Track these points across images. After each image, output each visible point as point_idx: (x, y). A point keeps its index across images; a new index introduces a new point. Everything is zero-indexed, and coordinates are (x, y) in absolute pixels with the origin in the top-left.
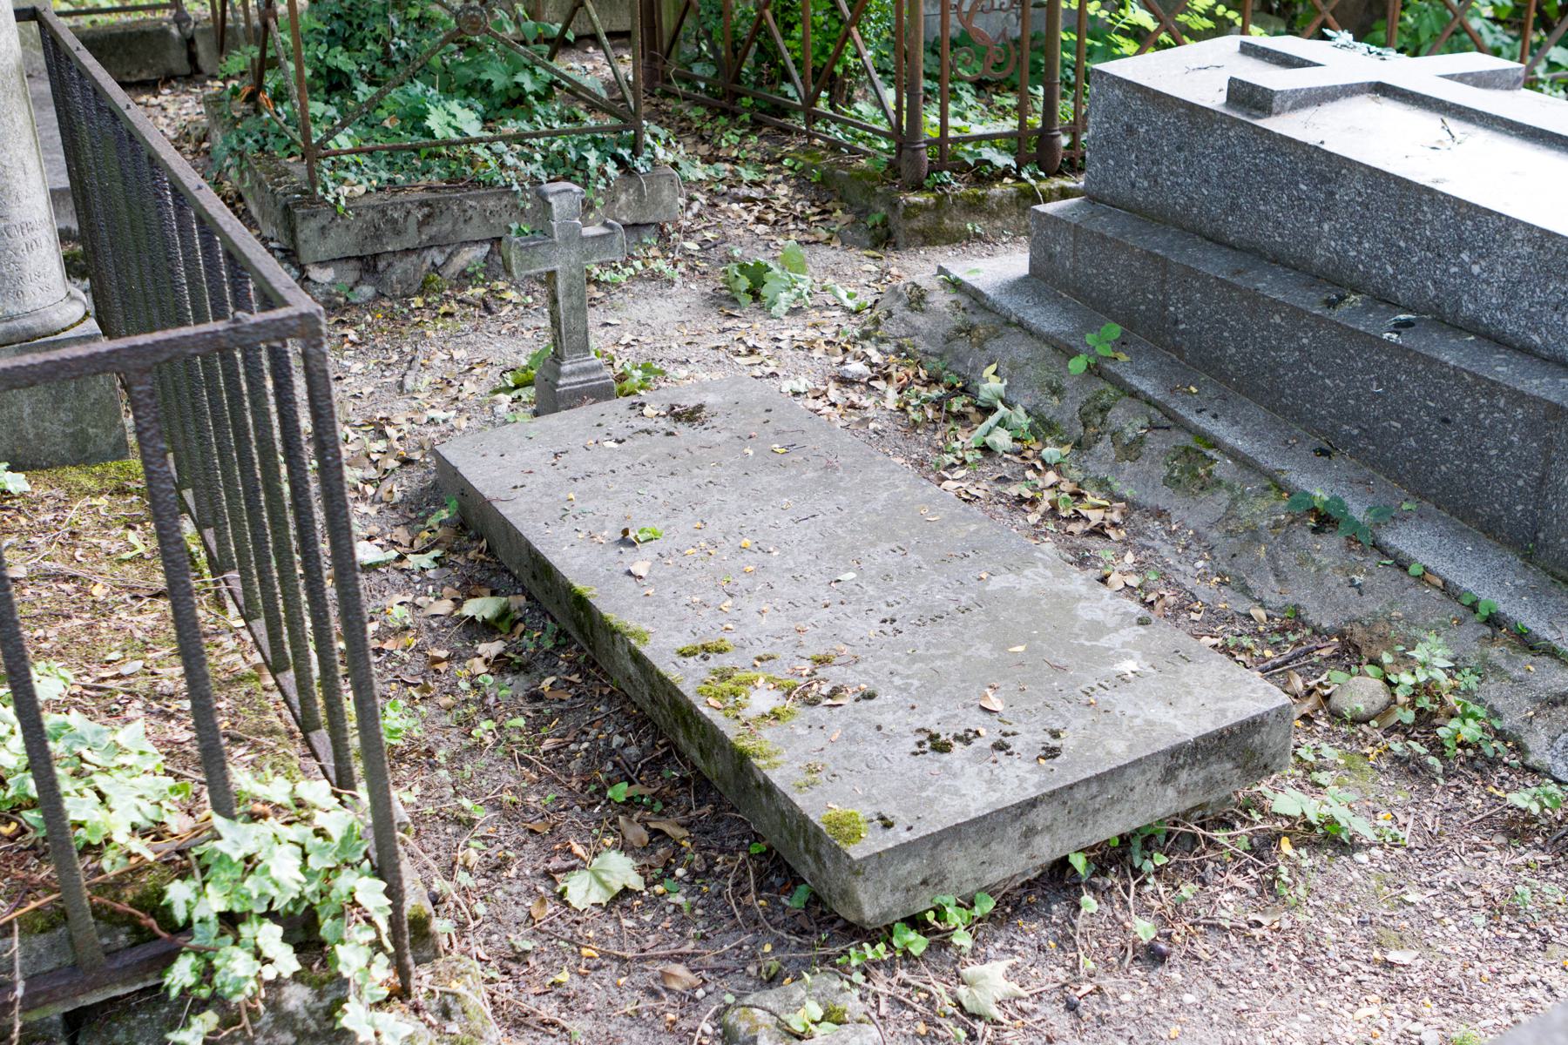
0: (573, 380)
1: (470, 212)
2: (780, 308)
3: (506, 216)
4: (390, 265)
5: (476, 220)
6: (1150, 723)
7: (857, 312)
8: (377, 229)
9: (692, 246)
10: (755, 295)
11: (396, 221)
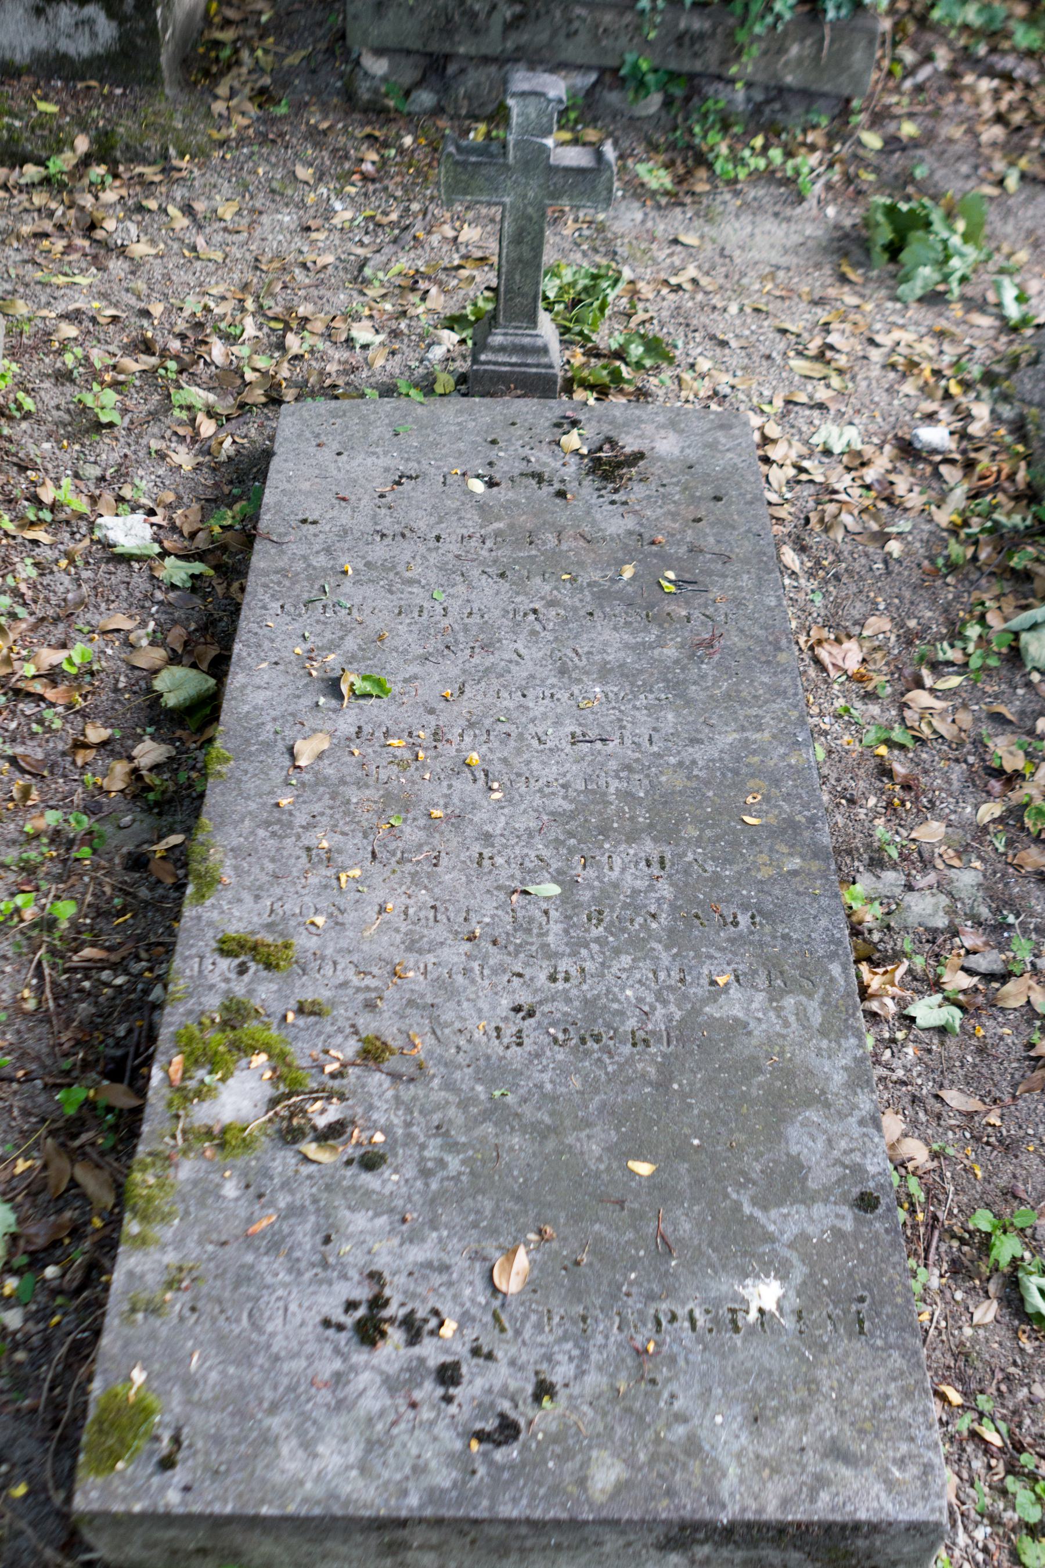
0: (501, 358)
1: (576, 24)
2: (916, 288)
3: (624, 40)
4: (462, 71)
5: (583, 38)
6: (693, 1446)
7: (1015, 329)
8: (449, 21)
9: (873, 140)
10: (894, 250)
11: (475, 15)
